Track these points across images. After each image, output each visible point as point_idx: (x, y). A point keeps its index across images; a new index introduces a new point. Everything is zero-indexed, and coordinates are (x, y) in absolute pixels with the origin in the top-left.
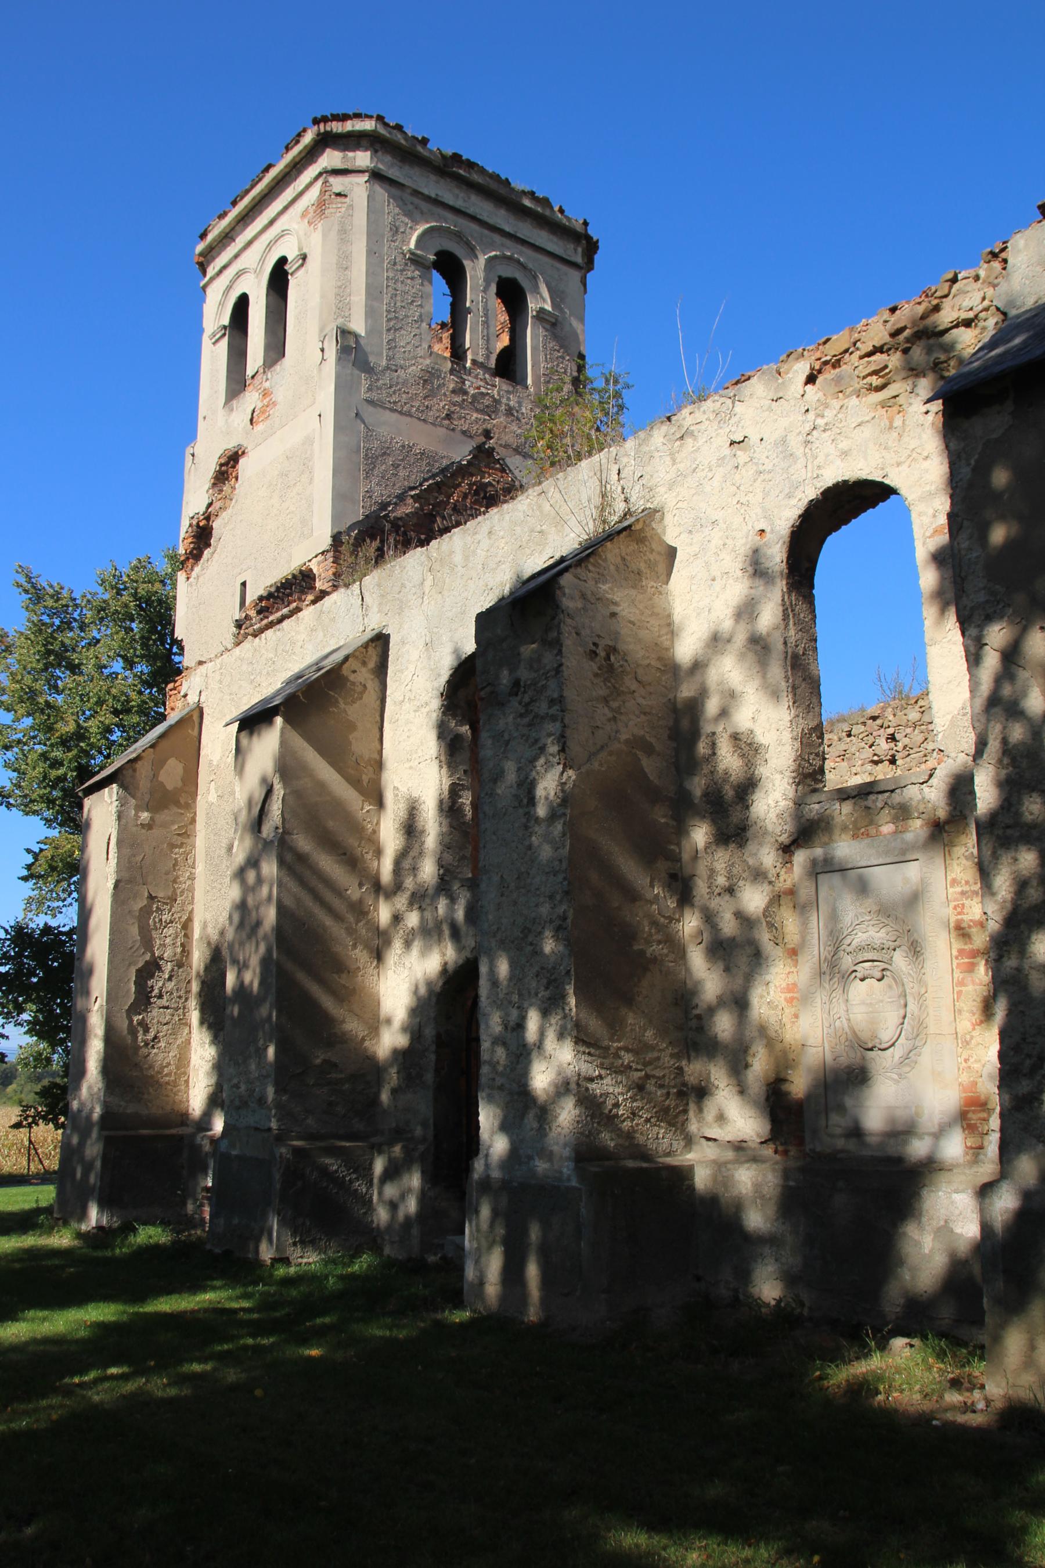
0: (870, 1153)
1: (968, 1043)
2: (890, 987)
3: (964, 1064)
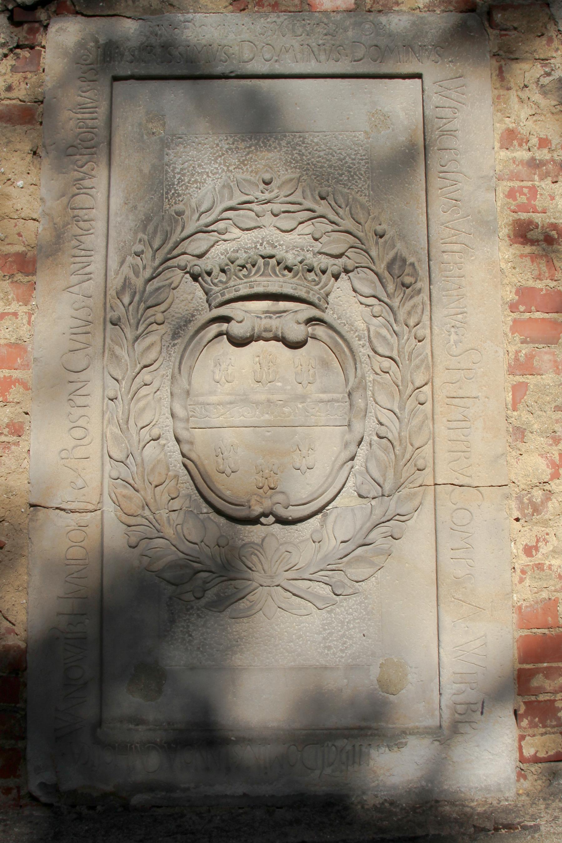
0: (237, 788)
1: (536, 510)
2: (325, 364)
3: (524, 560)
